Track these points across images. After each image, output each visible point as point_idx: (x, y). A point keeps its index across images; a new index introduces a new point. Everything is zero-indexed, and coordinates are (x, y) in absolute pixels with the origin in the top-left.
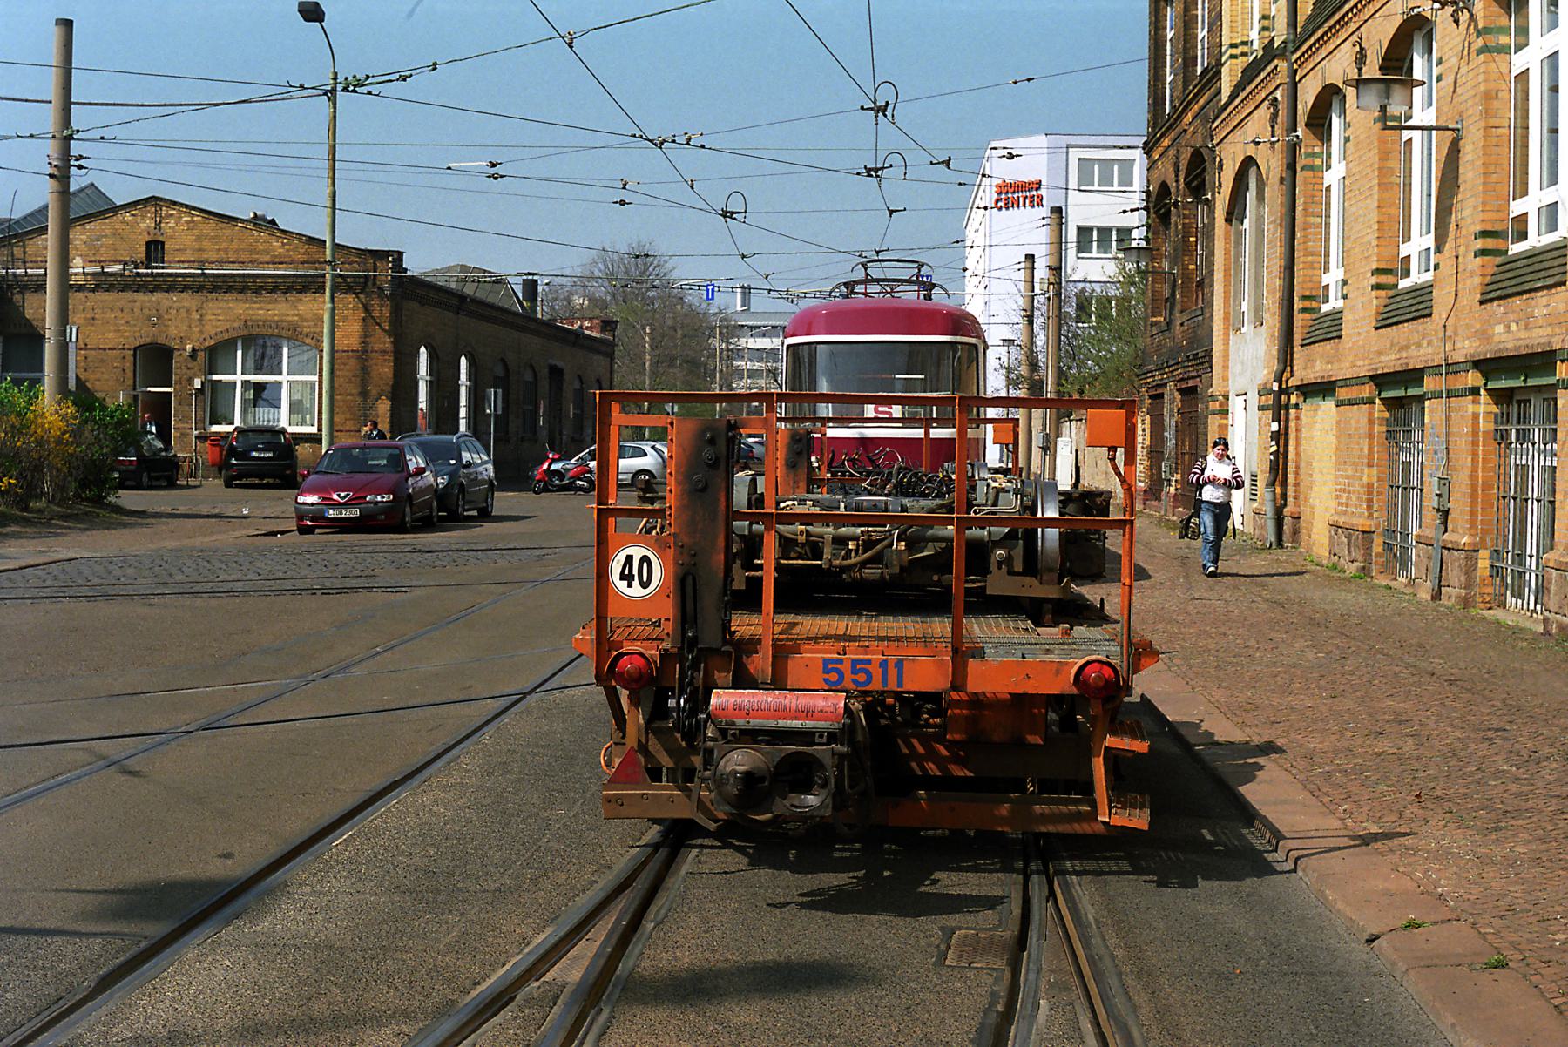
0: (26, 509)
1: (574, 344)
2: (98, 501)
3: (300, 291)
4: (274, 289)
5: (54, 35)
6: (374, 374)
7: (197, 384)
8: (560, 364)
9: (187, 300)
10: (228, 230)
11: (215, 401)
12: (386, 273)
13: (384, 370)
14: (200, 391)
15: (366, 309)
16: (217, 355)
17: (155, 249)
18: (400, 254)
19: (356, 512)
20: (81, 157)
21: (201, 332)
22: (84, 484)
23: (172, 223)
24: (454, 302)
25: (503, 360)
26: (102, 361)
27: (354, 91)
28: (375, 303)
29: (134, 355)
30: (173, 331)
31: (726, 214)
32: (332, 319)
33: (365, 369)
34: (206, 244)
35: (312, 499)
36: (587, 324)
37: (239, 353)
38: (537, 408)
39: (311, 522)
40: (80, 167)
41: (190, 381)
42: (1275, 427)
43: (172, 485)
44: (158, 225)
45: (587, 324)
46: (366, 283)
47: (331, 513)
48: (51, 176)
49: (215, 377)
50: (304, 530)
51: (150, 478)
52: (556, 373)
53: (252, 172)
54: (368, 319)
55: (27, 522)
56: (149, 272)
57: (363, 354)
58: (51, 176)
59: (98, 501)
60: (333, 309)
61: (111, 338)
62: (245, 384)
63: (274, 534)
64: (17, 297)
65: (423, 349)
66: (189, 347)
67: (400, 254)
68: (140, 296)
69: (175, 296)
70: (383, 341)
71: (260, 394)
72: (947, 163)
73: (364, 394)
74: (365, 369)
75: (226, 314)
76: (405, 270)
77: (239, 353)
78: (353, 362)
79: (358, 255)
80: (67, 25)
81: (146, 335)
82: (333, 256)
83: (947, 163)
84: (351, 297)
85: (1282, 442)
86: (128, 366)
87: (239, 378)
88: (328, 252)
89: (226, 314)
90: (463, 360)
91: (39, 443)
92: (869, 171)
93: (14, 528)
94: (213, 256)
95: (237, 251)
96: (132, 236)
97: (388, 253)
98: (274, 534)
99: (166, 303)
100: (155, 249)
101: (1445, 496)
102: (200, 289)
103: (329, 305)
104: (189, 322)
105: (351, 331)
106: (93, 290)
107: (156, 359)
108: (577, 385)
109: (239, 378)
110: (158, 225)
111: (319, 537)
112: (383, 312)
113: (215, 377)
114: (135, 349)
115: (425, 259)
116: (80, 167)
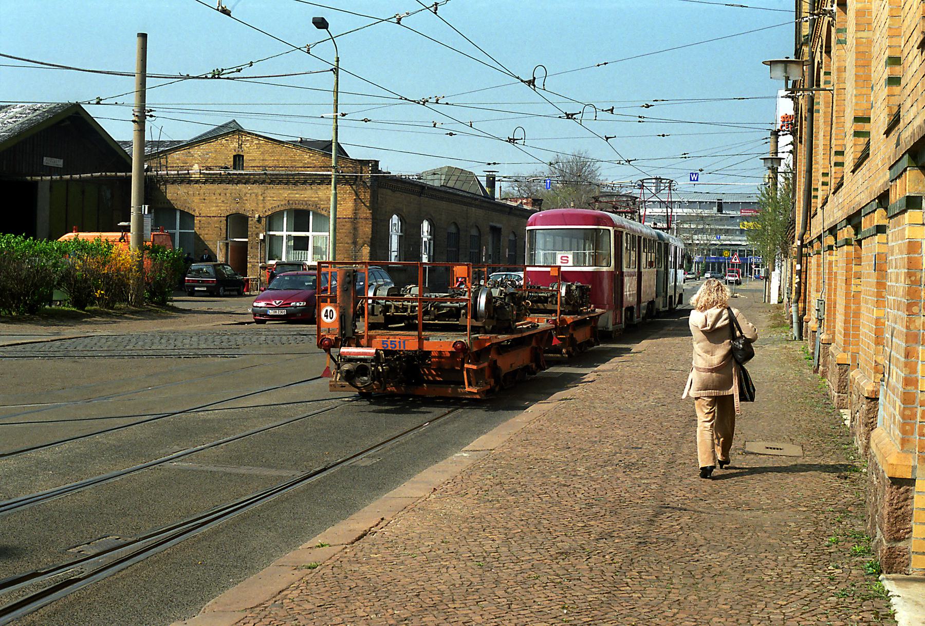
0: (112, 308)
1: (509, 213)
2: (162, 304)
3: (319, 184)
4: (304, 183)
5: (136, 42)
6: (360, 232)
7: (261, 237)
8: (498, 225)
9: (257, 189)
10: (279, 149)
11: (271, 244)
12: (367, 174)
13: (366, 229)
14: (263, 241)
15: (357, 195)
16: (272, 220)
17: (238, 160)
18: (377, 162)
19: (284, 312)
20: (151, 111)
21: (264, 207)
22: (153, 294)
23: (248, 145)
24: (417, 189)
25: (455, 224)
26: (209, 223)
27: (219, 78)
28: (362, 190)
29: (227, 220)
30: (248, 206)
31: (512, 141)
32: (335, 201)
33: (355, 229)
34: (267, 157)
35: (262, 304)
36: (524, 201)
37: (285, 219)
38: (480, 251)
39: (261, 318)
40: (151, 116)
41: (257, 235)
42: (798, 267)
43: (240, 294)
44: (240, 146)
45: (524, 201)
46: (356, 180)
47: (271, 312)
48: (134, 121)
49: (271, 233)
50: (258, 322)
51: (225, 291)
52: (496, 231)
53: (285, 114)
54: (358, 199)
55: (108, 315)
56: (235, 174)
57: (354, 220)
58: (134, 121)
59: (162, 304)
60: (336, 194)
61: (213, 210)
62: (289, 237)
63: (243, 323)
64: (163, 187)
65: (395, 217)
66: (257, 216)
67: (377, 162)
68: (230, 186)
69: (249, 187)
70: (365, 213)
71: (301, 244)
72: (612, 110)
73: (355, 243)
74: (355, 229)
75: (278, 197)
76: (380, 172)
77: (285, 219)
78: (349, 225)
79: (352, 163)
80: (144, 36)
81: (234, 208)
82: (337, 162)
83: (612, 110)
84: (348, 187)
85: (803, 276)
86: (223, 227)
87: (284, 233)
88: (333, 162)
89: (278, 197)
90: (425, 226)
91: (118, 270)
92: (568, 115)
93: (97, 319)
94: (270, 163)
95: (284, 161)
96: (226, 152)
97: (369, 162)
98: (243, 323)
99: (244, 191)
100: (238, 160)
101: (822, 310)
102: (263, 182)
103: (333, 192)
104: (258, 201)
105: (347, 207)
106: (204, 183)
107: (238, 222)
108: (512, 237)
109: (284, 233)
110: (240, 146)
111: (270, 325)
112: (366, 196)
113: (271, 233)
114: (227, 217)
115: (394, 165)
116: (151, 116)
